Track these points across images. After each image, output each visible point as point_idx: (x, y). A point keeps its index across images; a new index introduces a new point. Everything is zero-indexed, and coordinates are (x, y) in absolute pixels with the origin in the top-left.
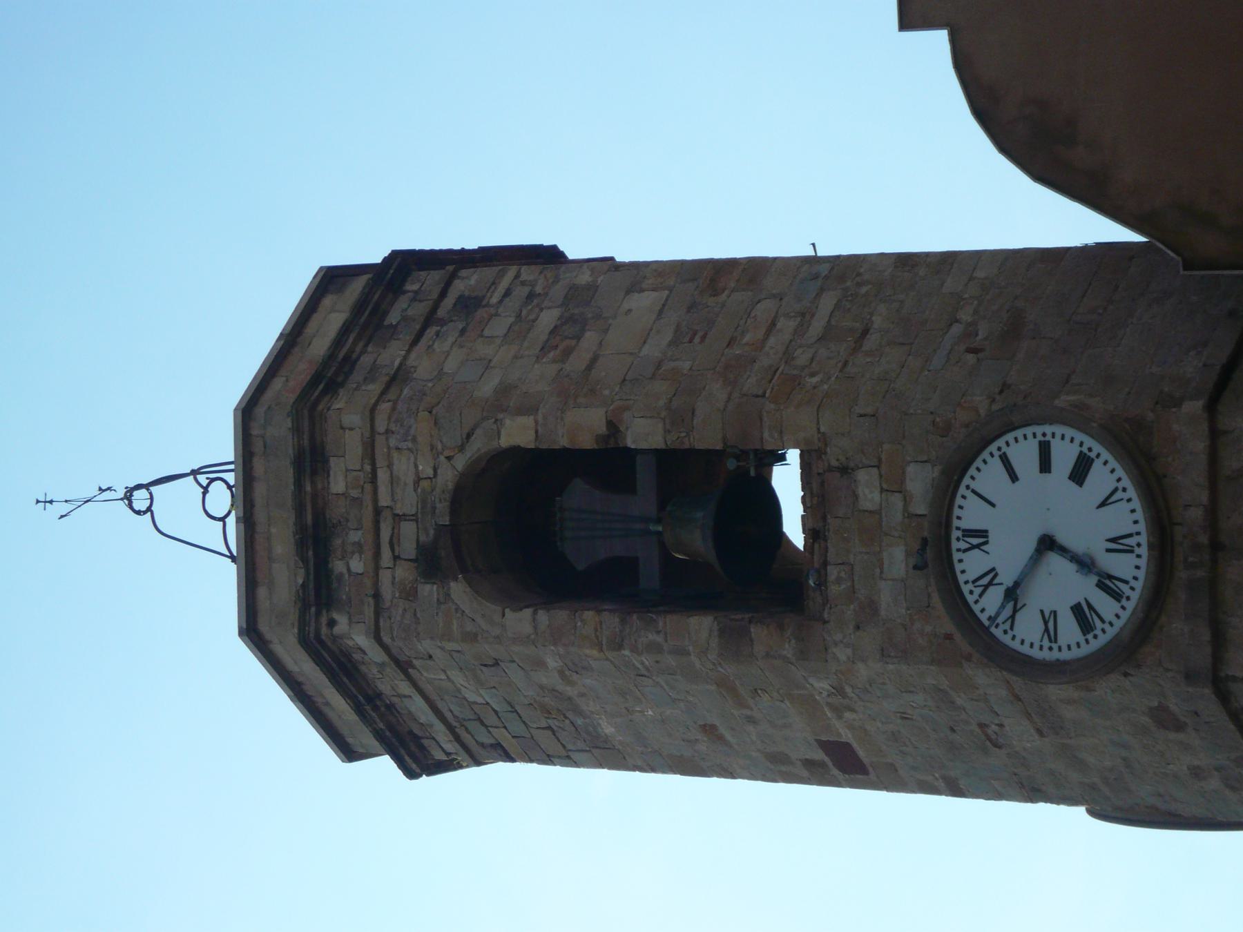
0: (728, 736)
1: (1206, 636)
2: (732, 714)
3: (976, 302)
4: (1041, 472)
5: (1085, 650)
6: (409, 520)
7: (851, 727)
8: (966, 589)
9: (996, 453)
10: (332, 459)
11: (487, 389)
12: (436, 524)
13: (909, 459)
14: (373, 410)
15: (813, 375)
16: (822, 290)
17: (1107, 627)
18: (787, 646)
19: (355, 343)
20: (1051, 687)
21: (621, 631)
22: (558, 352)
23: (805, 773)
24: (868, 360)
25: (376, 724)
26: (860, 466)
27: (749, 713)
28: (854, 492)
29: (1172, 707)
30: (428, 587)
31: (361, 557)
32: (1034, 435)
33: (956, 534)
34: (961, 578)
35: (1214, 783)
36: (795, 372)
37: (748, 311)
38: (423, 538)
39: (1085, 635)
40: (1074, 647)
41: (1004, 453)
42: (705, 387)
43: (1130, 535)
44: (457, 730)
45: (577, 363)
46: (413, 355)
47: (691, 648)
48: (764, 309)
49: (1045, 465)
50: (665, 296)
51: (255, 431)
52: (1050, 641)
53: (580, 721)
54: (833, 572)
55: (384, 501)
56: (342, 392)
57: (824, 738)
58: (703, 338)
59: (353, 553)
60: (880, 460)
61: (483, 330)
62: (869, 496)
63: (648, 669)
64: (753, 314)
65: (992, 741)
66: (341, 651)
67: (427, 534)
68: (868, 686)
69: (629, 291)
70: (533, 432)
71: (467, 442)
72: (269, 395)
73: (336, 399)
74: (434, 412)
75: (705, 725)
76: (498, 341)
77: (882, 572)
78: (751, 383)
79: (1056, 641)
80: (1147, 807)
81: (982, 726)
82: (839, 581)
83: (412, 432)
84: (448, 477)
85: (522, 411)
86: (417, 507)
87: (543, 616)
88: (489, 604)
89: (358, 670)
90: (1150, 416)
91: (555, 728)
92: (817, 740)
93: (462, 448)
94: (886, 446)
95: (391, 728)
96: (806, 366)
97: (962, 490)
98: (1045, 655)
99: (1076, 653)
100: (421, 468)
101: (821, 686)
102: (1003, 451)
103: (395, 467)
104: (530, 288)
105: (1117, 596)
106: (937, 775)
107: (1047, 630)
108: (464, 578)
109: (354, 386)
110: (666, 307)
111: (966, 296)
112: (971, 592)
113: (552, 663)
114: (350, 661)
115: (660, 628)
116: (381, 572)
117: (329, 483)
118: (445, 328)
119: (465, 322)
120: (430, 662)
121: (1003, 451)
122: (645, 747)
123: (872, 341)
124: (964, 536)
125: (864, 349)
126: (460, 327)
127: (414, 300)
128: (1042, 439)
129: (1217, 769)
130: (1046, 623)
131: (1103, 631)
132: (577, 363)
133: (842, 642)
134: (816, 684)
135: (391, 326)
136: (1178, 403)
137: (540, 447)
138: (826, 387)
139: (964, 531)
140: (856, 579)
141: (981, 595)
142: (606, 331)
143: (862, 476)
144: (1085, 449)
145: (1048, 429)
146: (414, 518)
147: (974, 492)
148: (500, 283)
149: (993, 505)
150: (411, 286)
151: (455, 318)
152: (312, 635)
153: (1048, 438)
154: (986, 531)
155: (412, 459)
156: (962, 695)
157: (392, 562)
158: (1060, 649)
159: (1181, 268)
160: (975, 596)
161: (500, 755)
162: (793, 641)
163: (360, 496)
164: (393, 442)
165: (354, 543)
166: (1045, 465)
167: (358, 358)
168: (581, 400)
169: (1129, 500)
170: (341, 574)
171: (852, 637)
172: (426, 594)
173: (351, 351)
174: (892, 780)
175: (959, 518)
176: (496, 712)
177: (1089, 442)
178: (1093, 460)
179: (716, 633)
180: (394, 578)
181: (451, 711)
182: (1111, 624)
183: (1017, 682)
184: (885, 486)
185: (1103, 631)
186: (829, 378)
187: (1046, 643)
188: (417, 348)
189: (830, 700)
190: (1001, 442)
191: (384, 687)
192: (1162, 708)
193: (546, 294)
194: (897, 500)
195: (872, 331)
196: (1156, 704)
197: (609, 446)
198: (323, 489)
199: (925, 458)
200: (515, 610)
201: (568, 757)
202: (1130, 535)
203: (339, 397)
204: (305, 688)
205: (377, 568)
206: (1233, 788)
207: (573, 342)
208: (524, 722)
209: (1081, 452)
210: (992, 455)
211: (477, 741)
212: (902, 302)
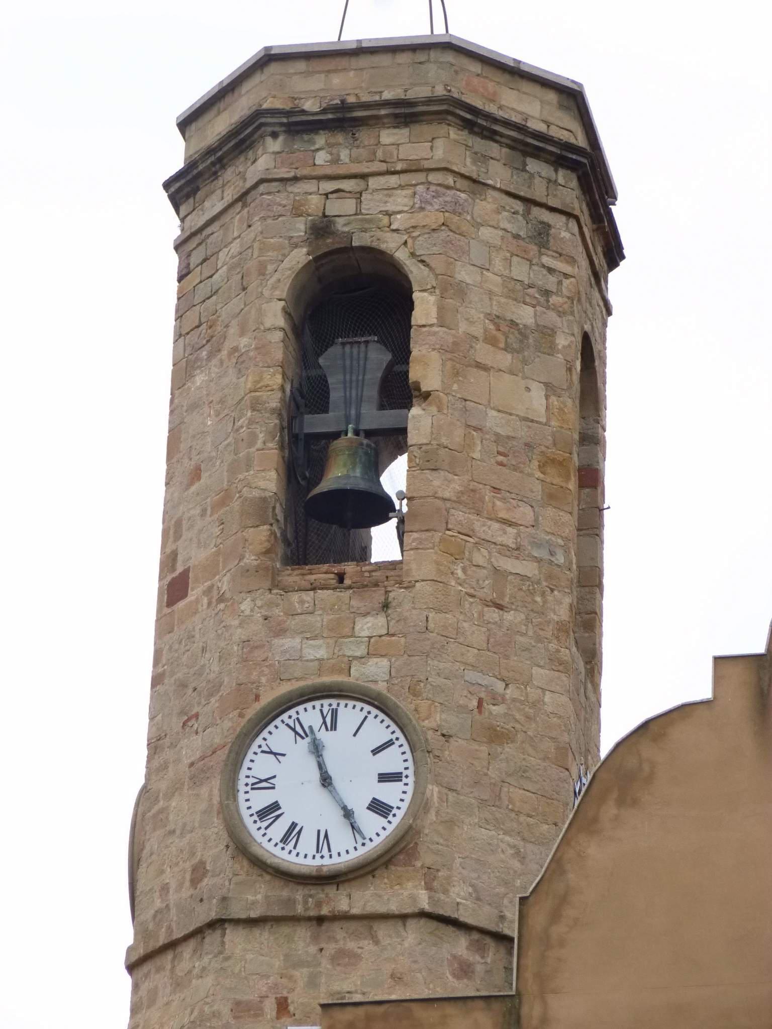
0: (193, 489)
1: (253, 915)
2: (207, 497)
3: (523, 698)
4: (379, 774)
5: (245, 813)
6: (357, 208)
7: (197, 601)
8: (292, 712)
9: (394, 737)
10: (408, 129)
11: (465, 274)
12: (353, 233)
13: (393, 660)
14: (446, 169)
15: (464, 570)
16: (539, 560)
17: (262, 831)
18: (253, 558)
19: (508, 137)
20: (218, 782)
21: (266, 409)
22: (494, 332)
23: (168, 551)
24: (475, 615)
25: (202, 163)
26: (389, 618)
27: (209, 512)
28: (369, 613)
29: (206, 880)
30: (302, 227)
31: (327, 162)
32: (406, 768)
33: (334, 702)
34: (300, 708)
35: (158, 904)
36: (467, 553)
37: (525, 499)
38: (340, 221)
39: (257, 813)
40: (248, 804)
41: (393, 743)
42: (456, 475)
43: (329, 850)
44: (199, 236)
45: (483, 352)
46: (496, 194)
47: (252, 472)
48: (524, 513)
49: (384, 778)
50: (541, 420)
51: (433, 54)
52: (253, 784)
53: (204, 354)
54: (308, 596)
55: (373, 182)
56: (465, 132)
57: (191, 575)
58: (501, 464)
59: (331, 154)
60: (393, 635)
61: (517, 256)
62: (365, 627)
63: (237, 430)
64: (520, 503)
65: (189, 719)
66: (254, 142)
67: (345, 225)
68: (224, 624)
69: (546, 384)
70: (423, 323)
71: (419, 261)
72: (465, 62)
73: (459, 129)
74: (443, 228)
75: (200, 470)
76: (506, 273)
77: (307, 638)
78: (459, 516)
79: (252, 789)
80: (143, 843)
81: (197, 716)
82: (302, 602)
83: (429, 207)
84: (390, 244)
85: (441, 309)
86: (367, 214)
87: (278, 335)
88: (288, 285)
89: (241, 152)
90: (419, 864)
91: (200, 328)
92: (189, 567)
93: (413, 255)
94: (403, 640)
95: (200, 175)
96: (472, 562)
97: (367, 708)
98: (242, 780)
99: (243, 806)
100: (399, 216)
101: (225, 585)
102: (396, 742)
103: (400, 191)
104: (555, 291)
105: (285, 839)
106: (166, 667)
107: (261, 781)
108: (310, 262)
109: (470, 144)
110: (530, 424)
111: (529, 689)
112: (290, 717)
113: (244, 341)
114: (247, 148)
115: (267, 444)
116: (315, 181)
117: (389, 128)
118: (520, 218)
119: (525, 236)
120: (245, 225)
121: (396, 742)
122: (186, 411)
123: (493, 614)
124: (333, 709)
125: (486, 609)
126: (521, 233)
127: (549, 181)
128: (404, 775)
129: (167, 906)
130: (266, 780)
131: (259, 829)
132: (483, 352)
133: (255, 605)
134: (225, 579)
135: (525, 165)
136: (429, 888)
137: (412, 330)
138: (453, 583)
139: (337, 710)
140: (303, 617)
141: (287, 725)
142: (512, 373)
143: (381, 620)
144: (394, 811)
145: (411, 780)
146: (358, 212)
147: (366, 718)
148: (561, 261)
149: (355, 735)
150: (562, 176)
151: (530, 226)
152: (263, 120)
153: (404, 780)
154: (335, 729)
155: (406, 209)
156: (217, 705)
157: (324, 192)
158: (247, 792)
159: (520, 896)
160: (287, 721)
161: (182, 271)
162: (255, 563)
163: (377, 159)
164: (420, 189)
165: (339, 156)
166: (384, 778)
167: (496, 141)
168: (449, 364)
169: (356, 849)
170: (314, 143)
171: (259, 615)
172: (297, 226)
173: (502, 135)
174: (164, 626)
175: (346, 706)
176: (211, 277)
177: (400, 814)
178: (386, 818)
179: (263, 495)
180: (311, 194)
181: (212, 234)
182: (264, 835)
183: (222, 755)
184: (372, 640)
185: (259, 829)
186: (460, 585)
187: (251, 781)
188: (504, 196)
189: (215, 587)
190: (402, 740)
191: (229, 174)
192: (205, 873)
193: (548, 308)
194: (361, 651)
195: (501, 612)
196: (208, 868)
197: (412, 391)
198: (384, 124)
199: (393, 674)
200: (285, 310)
201: (180, 335)
202: (329, 850)
203: (460, 132)
204: (230, 94)
205: (319, 178)
206: (155, 916)
207: (502, 345)
208: (204, 301)
209: (392, 808)
210: (393, 732)
211: (192, 251)
212: (525, 634)
